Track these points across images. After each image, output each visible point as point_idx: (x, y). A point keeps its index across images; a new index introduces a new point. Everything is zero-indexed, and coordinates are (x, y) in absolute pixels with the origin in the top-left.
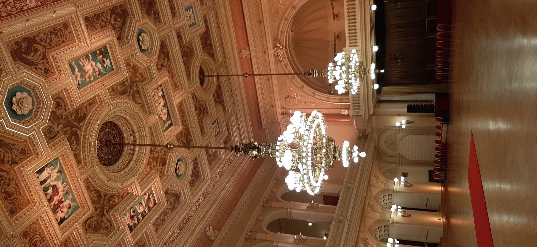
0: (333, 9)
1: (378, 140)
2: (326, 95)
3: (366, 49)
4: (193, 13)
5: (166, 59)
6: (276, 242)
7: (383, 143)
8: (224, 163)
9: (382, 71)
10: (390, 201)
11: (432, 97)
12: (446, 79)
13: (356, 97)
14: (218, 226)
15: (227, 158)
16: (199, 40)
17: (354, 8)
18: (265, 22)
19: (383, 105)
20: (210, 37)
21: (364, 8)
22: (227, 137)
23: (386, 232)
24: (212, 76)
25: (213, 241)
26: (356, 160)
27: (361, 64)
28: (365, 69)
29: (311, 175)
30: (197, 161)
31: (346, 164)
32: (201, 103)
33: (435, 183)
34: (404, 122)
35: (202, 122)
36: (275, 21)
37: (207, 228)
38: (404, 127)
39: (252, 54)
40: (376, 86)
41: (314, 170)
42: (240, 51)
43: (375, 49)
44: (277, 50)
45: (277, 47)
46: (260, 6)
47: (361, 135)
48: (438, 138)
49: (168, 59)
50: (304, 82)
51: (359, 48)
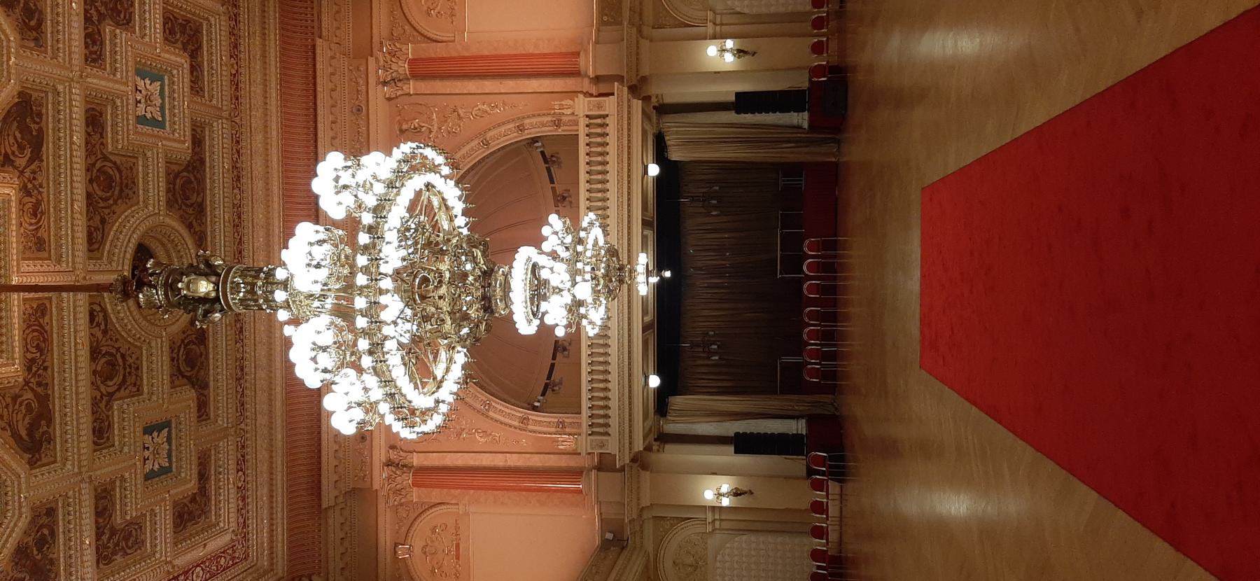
0: (552, 181)
1: (657, 551)
2: (520, 412)
4: (169, 441)
5: (28, 152)
7: (668, 564)
9: (668, 274)
11: (797, 427)
12: (832, 381)
27: (612, 252)
30: (55, 522)
35: (109, 406)
47: (609, 536)
48: (819, 544)
49: (36, 156)
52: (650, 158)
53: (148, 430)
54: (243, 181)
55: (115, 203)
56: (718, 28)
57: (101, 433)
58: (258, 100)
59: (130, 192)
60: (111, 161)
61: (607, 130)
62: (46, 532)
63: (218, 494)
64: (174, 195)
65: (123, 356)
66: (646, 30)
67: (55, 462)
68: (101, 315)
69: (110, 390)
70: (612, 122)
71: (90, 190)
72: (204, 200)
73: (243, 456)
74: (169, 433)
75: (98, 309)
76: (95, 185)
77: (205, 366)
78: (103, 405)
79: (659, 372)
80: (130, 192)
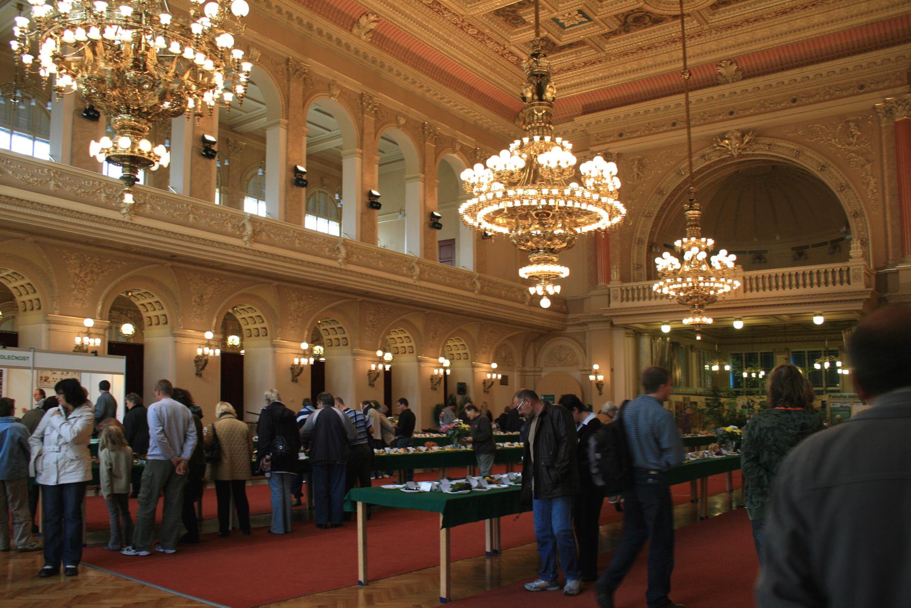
3: (734, 306)
6: (362, 154)
8: (501, 41)
10: (456, 357)
13: (650, 294)
14: (379, 38)
15: (513, 49)
17: (770, 288)
19: (630, 342)
21: (817, 302)
22: (554, 44)
23: (401, 350)
25: (351, 30)
26: (532, 290)
27: (712, 300)
28: (701, 306)
29: (495, 207)
31: (524, 272)
33: (189, 179)
34: (600, 378)
37: (372, 18)
38: (592, 378)
39: (728, 86)
40: (666, 329)
41: (512, 211)
42: (732, 61)
44: (737, 138)
45: (743, 136)
46: (827, 97)
50: (673, 195)
51: (741, 295)
52: (199, 334)
53: (580, 12)
54: (784, 17)
61: (831, 285)
63: (564, 56)
70: (845, 287)
77: (639, 28)
79: (747, 327)
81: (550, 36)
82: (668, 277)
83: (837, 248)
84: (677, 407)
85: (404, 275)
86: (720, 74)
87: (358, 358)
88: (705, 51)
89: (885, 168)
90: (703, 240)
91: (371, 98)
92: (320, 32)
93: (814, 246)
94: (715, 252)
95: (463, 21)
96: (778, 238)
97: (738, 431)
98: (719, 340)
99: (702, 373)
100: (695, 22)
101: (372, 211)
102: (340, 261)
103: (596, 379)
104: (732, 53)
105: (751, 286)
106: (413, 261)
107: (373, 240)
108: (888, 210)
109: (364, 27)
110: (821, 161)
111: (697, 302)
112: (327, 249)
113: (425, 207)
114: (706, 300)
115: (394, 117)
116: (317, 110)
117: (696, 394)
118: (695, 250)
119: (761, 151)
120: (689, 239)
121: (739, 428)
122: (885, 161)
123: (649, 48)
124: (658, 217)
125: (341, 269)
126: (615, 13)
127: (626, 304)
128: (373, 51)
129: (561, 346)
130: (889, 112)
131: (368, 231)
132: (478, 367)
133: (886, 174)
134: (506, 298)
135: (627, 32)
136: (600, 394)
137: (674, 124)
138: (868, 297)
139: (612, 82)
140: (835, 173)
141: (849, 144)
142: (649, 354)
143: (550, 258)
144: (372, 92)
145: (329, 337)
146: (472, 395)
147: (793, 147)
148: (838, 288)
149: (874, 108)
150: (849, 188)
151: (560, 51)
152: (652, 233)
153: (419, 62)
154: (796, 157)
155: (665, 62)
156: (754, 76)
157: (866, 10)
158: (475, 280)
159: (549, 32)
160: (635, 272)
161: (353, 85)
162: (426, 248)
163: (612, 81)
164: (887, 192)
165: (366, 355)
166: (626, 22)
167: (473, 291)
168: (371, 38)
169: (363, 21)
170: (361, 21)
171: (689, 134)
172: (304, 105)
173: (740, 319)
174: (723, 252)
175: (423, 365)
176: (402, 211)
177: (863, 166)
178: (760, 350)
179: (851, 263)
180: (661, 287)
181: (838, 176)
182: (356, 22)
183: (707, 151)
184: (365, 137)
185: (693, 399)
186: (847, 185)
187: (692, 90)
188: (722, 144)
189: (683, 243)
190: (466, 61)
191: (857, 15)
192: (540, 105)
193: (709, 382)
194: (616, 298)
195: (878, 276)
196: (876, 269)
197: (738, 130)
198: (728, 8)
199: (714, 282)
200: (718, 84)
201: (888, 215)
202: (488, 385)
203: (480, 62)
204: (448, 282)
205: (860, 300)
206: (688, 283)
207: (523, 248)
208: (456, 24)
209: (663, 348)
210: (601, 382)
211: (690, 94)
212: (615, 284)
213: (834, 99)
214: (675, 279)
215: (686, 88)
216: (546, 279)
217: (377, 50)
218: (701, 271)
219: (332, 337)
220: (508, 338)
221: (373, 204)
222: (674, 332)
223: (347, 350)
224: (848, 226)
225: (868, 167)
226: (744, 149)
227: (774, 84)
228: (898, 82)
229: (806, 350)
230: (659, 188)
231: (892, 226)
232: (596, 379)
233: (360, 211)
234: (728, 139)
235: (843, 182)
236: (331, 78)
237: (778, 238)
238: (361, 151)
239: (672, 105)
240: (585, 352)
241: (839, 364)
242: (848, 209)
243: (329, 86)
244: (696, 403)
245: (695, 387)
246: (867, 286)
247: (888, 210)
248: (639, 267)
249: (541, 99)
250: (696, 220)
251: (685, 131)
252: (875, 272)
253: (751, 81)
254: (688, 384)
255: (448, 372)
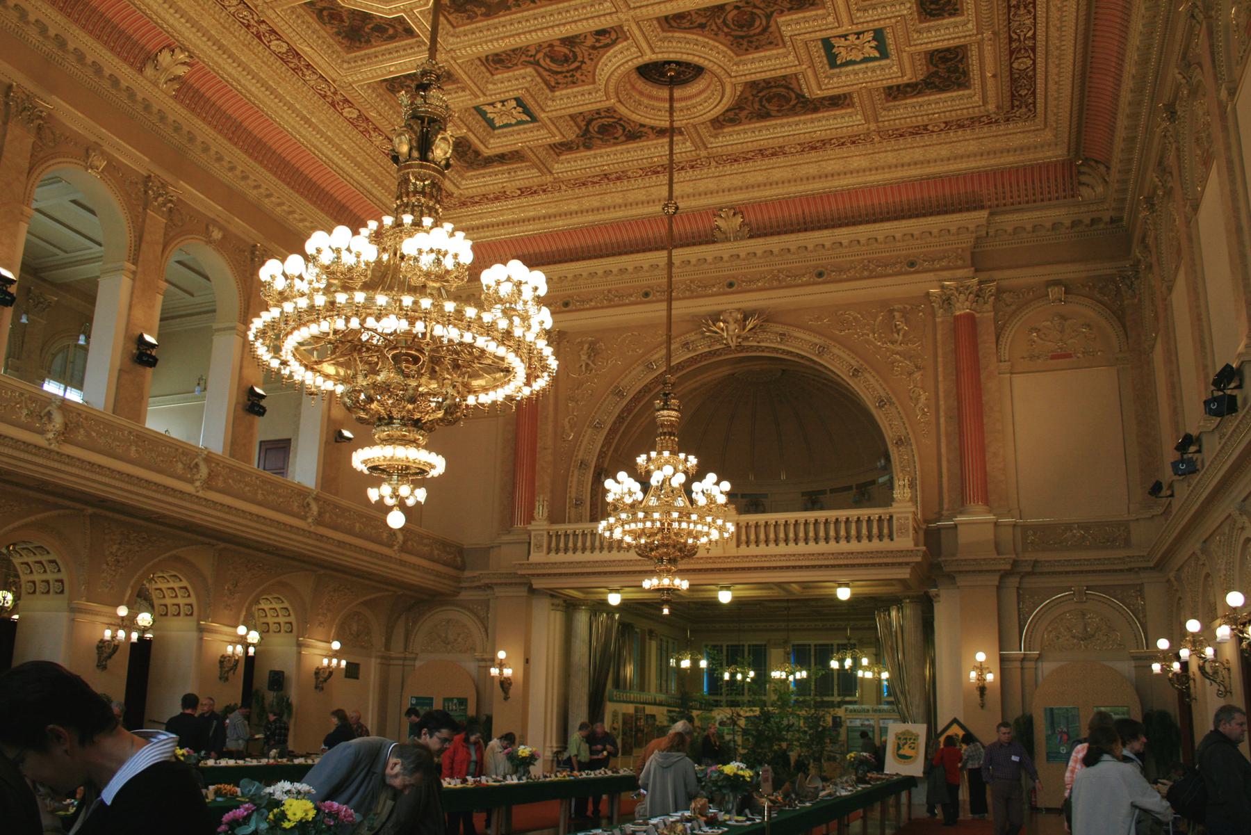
1: (469, 610)
3: (722, 569)
4: (865, 60)
6: (134, 273)
9: (666, 611)
10: (273, 627)
14: (188, 92)
16: (779, 73)
18: (821, 287)
19: (557, 618)
20: (786, 116)
21: (845, 565)
22: (477, 153)
23: (172, 610)
24: (671, 110)
25: (141, 70)
26: (373, 494)
27: (690, 552)
28: (672, 561)
32: (588, 66)
34: (508, 672)
35: (526, 64)
36: (819, 318)
37: (182, 57)
38: (494, 671)
39: (728, 245)
40: (614, 599)
42: (736, 210)
43: (725, 597)
44: (736, 321)
45: (745, 319)
46: (866, 273)
51: (732, 550)
53: (519, 102)
54: (813, 153)
55: (727, 34)
56: (1018, 664)
57: (498, 62)
58: (906, 157)
59: (745, 46)
60: (768, 23)
62: (391, 31)
64: (763, 88)
65: (579, 68)
66: (1013, 582)
67: (454, 27)
68: (608, 41)
69: (542, 62)
70: (886, 545)
71: (728, 8)
72: (775, 117)
73: (535, 192)
74: (875, 59)
75: (614, 36)
76: (735, 12)
77: (605, 143)
78: (524, 58)
79: (737, 603)
80: (745, 46)
81: (471, 137)
82: (623, 510)
83: (869, 490)
84: (625, 723)
85: (179, 478)
86: (718, 227)
87: (82, 618)
88: (699, 191)
89: (940, 378)
90: (682, 456)
91: (164, 186)
92: (81, 57)
93: (832, 491)
94: (699, 475)
95: (335, 93)
96: (783, 477)
97: (748, 774)
98: (694, 620)
99: (664, 670)
100: (688, 144)
101: (140, 369)
102: (51, 435)
103: (501, 673)
104: (737, 197)
105: (748, 537)
106: (197, 455)
107: (138, 414)
108: (943, 439)
109: (166, 70)
110: (853, 362)
111: (667, 554)
112: (25, 412)
113: (241, 378)
114: (680, 550)
115: (203, 226)
116: (74, 202)
117: (655, 704)
118: (668, 470)
119: (769, 342)
120: (660, 453)
121: (750, 767)
122: (940, 369)
123: (618, 178)
124: (613, 431)
125: (51, 451)
126: (572, 111)
127: (553, 557)
128: (177, 112)
129: (448, 621)
130: (947, 301)
131: (129, 400)
132: (308, 646)
133: (941, 386)
134: (360, 536)
135: (588, 148)
136: (506, 698)
137: (646, 295)
138: (919, 559)
139: (560, 223)
140: (872, 381)
141: (892, 343)
142: (587, 638)
143: (411, 436)
144: (166, 177)
145: (30, 578)
146: (293, 694)
147: (816, 341)
148: (876, 545)
149: (928, 294)
150: (892, 404)
151: (484, 167)
152: (602, 454)
153: (257, 148)
154: (820, 354)
155: (641, 201)
156: (766, 235)
157: (922, 158)
158: (309, 500)
159: (470, 130)
160: (573, 510)
161: (136, 160)
162: (237, 443)
163: (560, 223)
164: (942, 413)
165: (97, 614)
166: (587, 131)
167: (304, 518)
168: (178, 90)
169: (165, 57)
170: (160, 58)
171: (670, 309)
172: (31, 170)
173: (728, 588)
174: (712, 477)
175: (207, 637)
176: (202, 383)
177: (910, 374)
178: (749, 640)
179: (895, 509)
180: (611, 529)
181: (878, 387)
182: (151, 58)
183: (692, 337)
184: (144, 246)
185: (649, 710)
186: (889, 400)
187: (676, 247)
188: (714, 329)
189: (649, 459)
190: (336, 159)
191: (909, 165)
192: (422, 166)
193: (673, 686)
194: (539, 547)
195: (928, 532)
196: (926, 521)
197: (738, 310)
198: (736, 128)
199: (695, 523)
200: (714, 242)
201: (943, 445)
202: (323, 677)
203: (358, 165)
204: (260, 497)
205: (907, 564)
206: (653, 522)
207: (363, 415)
208: (325, 97)
209: (608, 630)
210: (508, 679)
211: (675, 252)
212: (540, 525)
213: (875, 277)
214: (634, 514)
215: (671, 242)
216: (399, 474)
217: (184, 112)
218: (673, 509)
219: (37, 577)
220: (365, 603)
221: (144, 356)
222: (625, 606)
223: (61, 601)
224: (888, 459)
225: (918, 375)
226: (746, 339)
227: (793, 248)
228: (960, 263)
229: (813, 643)
230: (617, 387)
231: (948, 461)
232: (501, 673)
233: (117, 364)
234: (724, 322)
235: (882, 393)
236: (93, 138)
237: (783, 477)
238: (133, 267)
239: (646, 266)
240: (486, 631)
241: (865, 661)
242: (889, 435)
243: (86, 151)
244: (653, 716)
245: (653, 692)
246: (916, 545)
247: (943, 439)
248: (579, 503)
249: (424, 157)
250: (672, 425)
251: (664, 306)
252: (924, 527)
253: (761, 241)
254: (642, 687)
255: (251, 651)
